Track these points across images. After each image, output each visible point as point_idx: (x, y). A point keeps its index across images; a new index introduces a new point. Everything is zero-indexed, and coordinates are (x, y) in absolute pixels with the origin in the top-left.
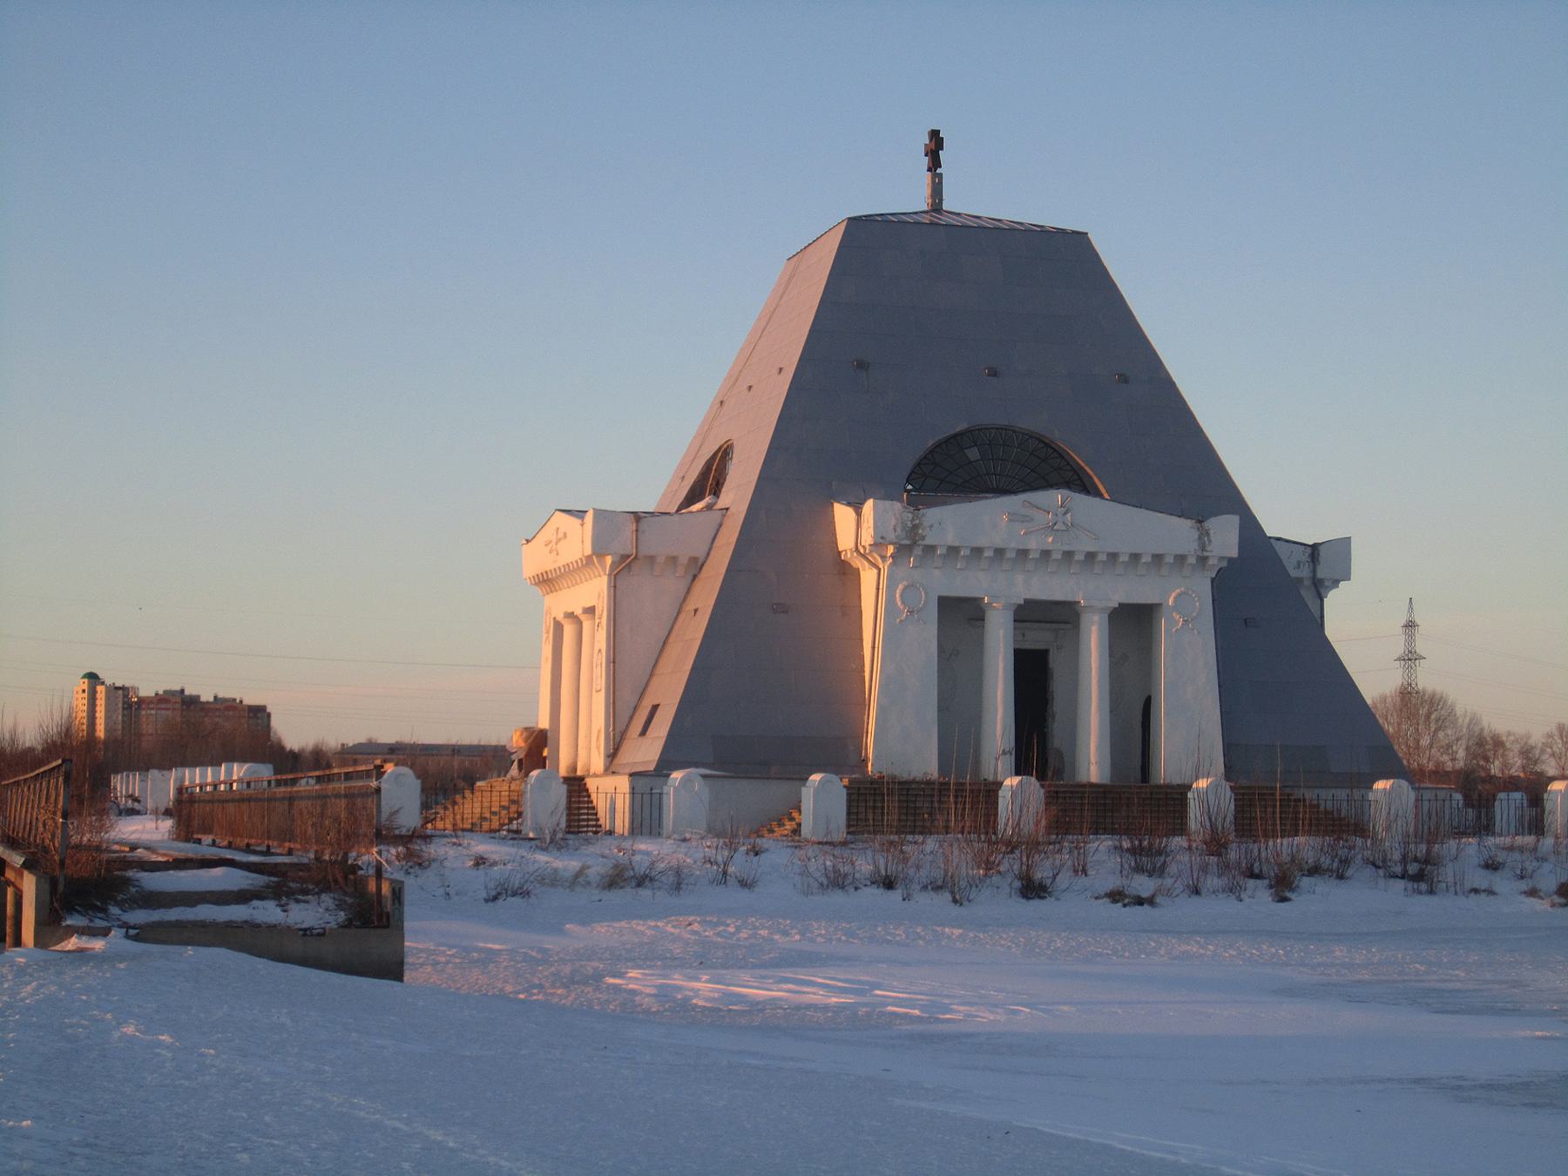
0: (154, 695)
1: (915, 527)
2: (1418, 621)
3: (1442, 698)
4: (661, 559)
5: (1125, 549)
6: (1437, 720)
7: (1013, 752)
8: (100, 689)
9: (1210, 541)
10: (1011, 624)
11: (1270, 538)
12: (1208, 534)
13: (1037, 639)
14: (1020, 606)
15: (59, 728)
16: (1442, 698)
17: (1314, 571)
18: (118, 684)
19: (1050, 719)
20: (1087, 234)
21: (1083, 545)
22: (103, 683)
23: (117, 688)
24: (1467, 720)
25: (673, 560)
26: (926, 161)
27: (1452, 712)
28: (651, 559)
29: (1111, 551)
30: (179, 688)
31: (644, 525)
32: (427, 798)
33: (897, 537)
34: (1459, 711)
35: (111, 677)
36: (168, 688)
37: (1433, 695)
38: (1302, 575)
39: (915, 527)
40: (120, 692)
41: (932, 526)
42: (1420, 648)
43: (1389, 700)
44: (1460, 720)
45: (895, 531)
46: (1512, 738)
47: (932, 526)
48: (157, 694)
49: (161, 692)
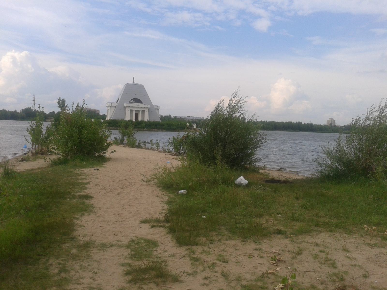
5: (141, 107)
20: (143, 85)
21: (139, 107)
25: (114, 106)
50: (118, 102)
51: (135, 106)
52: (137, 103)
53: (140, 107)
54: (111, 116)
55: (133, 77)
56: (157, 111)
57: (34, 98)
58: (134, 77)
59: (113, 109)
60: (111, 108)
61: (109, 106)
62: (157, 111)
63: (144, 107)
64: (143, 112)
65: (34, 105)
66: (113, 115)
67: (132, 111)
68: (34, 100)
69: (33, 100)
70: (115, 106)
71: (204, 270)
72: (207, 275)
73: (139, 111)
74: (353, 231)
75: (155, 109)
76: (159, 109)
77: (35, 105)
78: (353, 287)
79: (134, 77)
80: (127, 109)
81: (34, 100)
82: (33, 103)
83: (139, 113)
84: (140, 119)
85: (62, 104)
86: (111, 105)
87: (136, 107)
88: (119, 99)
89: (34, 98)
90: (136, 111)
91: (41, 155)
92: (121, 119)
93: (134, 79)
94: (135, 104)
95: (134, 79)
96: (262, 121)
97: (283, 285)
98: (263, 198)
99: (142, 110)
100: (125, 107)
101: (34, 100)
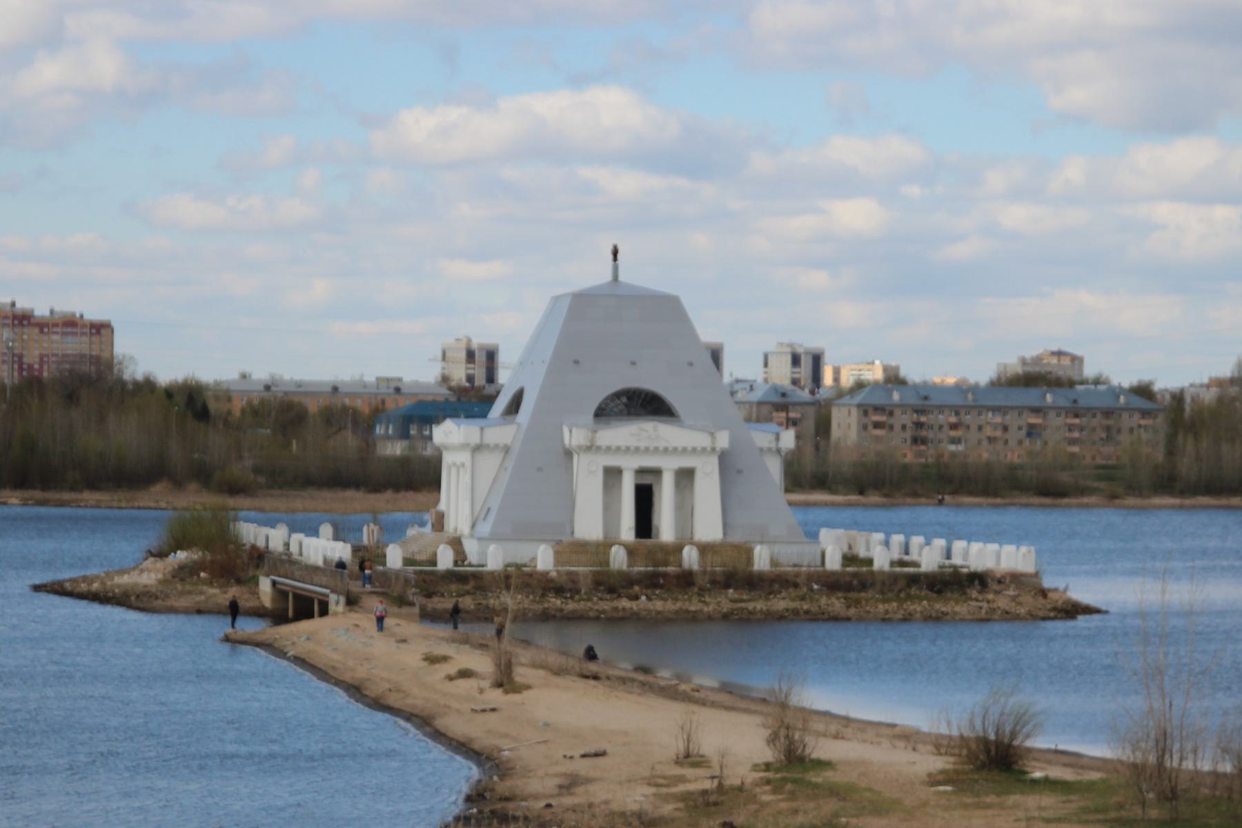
5: (671, 445)
13: (646, 480)
21: (661, 445)
25: (497, 446)
51: (633, 443)
54: (478, 508)
61: (468, 445)
63: (690, 445)
64: (685, 477)
67: (612, 475)
71: (25, 322)
73: (657, 472)
75: (761, 450)
81: (493, 710)
84: (666, 528)
85: (52, 312)
90: (641, 472)
91: (33, 365)
92: (216, 382)
96: (914, 373)
97: (209, 557)
98: (500, 588)
100: (568, 454)
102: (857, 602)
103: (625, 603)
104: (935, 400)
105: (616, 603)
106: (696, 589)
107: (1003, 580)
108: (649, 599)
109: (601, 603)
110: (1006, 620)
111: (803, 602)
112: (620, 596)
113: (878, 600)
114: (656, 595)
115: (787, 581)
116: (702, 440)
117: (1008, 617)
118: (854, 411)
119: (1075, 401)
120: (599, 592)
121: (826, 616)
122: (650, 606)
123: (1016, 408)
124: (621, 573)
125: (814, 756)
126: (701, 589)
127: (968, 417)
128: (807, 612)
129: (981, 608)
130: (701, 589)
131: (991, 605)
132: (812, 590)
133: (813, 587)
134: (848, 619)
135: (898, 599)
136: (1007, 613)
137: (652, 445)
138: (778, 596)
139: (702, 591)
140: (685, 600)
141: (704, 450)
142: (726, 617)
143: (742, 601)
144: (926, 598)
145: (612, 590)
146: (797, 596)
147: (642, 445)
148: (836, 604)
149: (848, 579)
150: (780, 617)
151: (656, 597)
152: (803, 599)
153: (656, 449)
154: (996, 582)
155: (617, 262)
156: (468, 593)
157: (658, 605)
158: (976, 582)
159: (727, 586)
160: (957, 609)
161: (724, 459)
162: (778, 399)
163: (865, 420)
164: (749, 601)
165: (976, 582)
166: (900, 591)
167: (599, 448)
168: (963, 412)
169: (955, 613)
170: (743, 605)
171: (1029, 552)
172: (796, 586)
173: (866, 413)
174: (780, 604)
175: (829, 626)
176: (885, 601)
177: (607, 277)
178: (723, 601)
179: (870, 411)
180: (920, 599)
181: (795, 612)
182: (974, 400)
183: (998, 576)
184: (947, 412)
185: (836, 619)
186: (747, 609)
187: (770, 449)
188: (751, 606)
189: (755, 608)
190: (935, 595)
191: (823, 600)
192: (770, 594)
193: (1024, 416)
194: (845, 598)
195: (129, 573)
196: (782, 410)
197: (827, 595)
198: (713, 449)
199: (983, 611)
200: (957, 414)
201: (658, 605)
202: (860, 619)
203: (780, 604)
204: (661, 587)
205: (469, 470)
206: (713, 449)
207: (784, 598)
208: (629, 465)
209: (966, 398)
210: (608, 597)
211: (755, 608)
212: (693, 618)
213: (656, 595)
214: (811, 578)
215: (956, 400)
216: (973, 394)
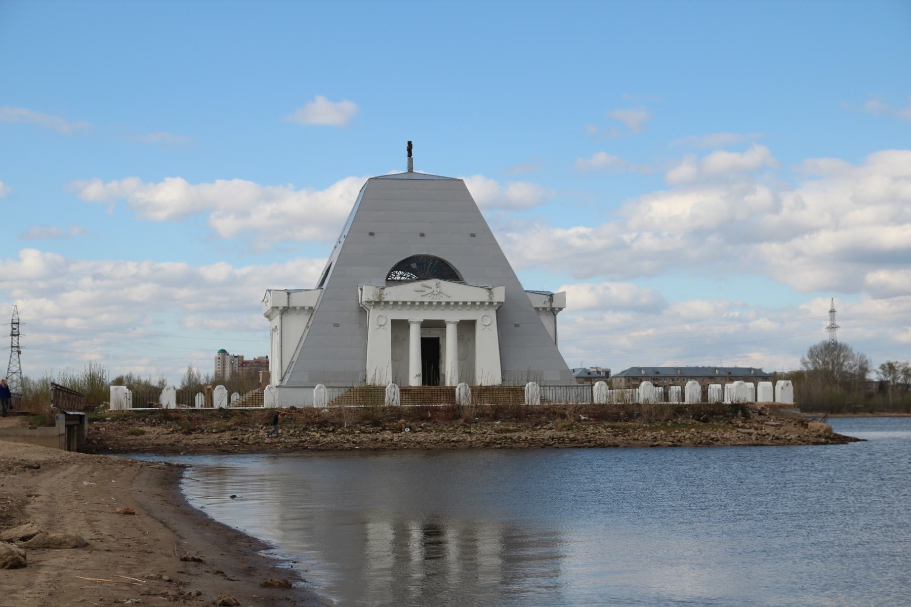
0: (253, 359)
1: (381, 295)
2: (836, 310)
3: (845, 346)
4: (298, 308)
5: (453, 300)
6: (844, 356)
7: (421, 375)
8: (227, 357)
9: (493, 296)
10: (420, 328)
11: (526, 291)
12: (493, 294)
13: (433, 334)
14: (422, 322)
15: (91, 377)
16: (845, 346)
17: (551, 305)
18: (236, 355)
19: (440, 363)
20: (462, 180)
21: (444, 300)
22: (228, 354)
23: (235, 357)
24: (859, 357)
25: (303, 308)
26: (407, 153)
27: (851, 350)
28: (295, 308)
29: (455, 301)
30: (265, 356)
31: (292, 295)
32: (443, 411)
33: (374, 298)
34: (855, 352)
35: (233, 351)
36: (260, 356)
37: (814, 346)
38: (546, 306)
39: (381, 295)
40: (237, 359)
41: (387, 294)
42: (838, 323)
43: (819, 348)
44: (856, 356)
45: (373, 296)
46: (897, 365)
47: (387, 294)
48: (255, 359)
49: (256, 358)
50: (325, 286)
51: (418, 298)
52: (432, 283)
53: (448, 303)
54: (285, 369)
55: (407, 145)
56: (546, 320)
57: (15, 326)
58: (410, 143)
59: (297, 326)
60: (285, 318)
61: (277, 308)
62: (546, 320)
64: (467, 328)
65: (15, 356)
66: (295, 359)
67: (400, 327)
68: (15, 334)
69: (13, 335)
70: (311, 308)
72: (723, 503)
74: (89, 432)
75: (537, 309)
76: (561, 309)
77: (19, 353)
78: (536, 544)
79: (410, 143)
80: (374, 315)
82: (12, 347)
83: (444, 336)
86: (283, 303)
87: (422, 303)
88: (331, 264)
89: (15, 326)
93: (410, 154)
94: (418, 285)
95: (410, 154)
99: (461, 321)
100: (362, 311)
101: (15, 332)
102: (625, 430)
103: (387, 435)
104: (662, 374)
105: (380, 436)
106: (462, 421)
107: (763, 412)
108: (412, 430)
109: (362, 435)
110: (778, 445)
111: (569, 432)
112: (384, 429)
113: (645, 429)
114: (421, 427)
115: (555, 413)
116: (481, 295)
117: (778, 442)
118: (623, 380)
119: (730, 373)
120: (363, 426)
121: (592, 444)
122: (411, 436)
123: (701, 377)
124: (393, 408)
125: (700, 398)
126: (467, 420)
127: (678, 381)
128: (573, 440)
129: (750, 434)
130: (467, 420)
131: (759, 432)
132: (579, 420)
133: (580, 418)
134: (616, 446)
135: (665, 427)
136: (777, 438)
137: (436, 299)
138: (545, 427)
139: (468, 422)
140: (450, 431)
141: (482, 303)
142: (488, 446)
143: (509, 431)
144: (693, 426)
145: (376, 423)
146: (565, 426)
147: (426, 299)
148: (603, 432)
149: (615, 410)
150: (545, 446)
151: (420, 429)
152: (570, 428)
153: (439, 303)
154: (757, 414)
155: (412, 157)
156: (229, 428)
157: (421, 436)
158: (740, 413)
159: (496, 418)
160: (727, 435)
161: (501, 310)
162: (587, 375)
163: (628, 384)
164: (515, 431)
165: (740, 413)
166: (667, 420)
167: (387, 303)
168: (676, 379)
169: (727, 439)
170: (508, 435)
171: (787, 385)
172: (563, 416)
173: (629, 380)
174: (545, 434)
175: (598, 453)
176: (651, 429)
177: (402, 169)
178: (489, 431)
179: (631, 379)
180: (687, 427)
181: (561, 440)
182: (681, 374)
183: (759, 408)
184: (668, 379)
185: (603, 446)
186: (511, 439)
187: (544, 309)
188: (516, 435)
189: (520, 437)
190: (702, 424)
191: (591, 429)
192: (536, 425)
193: (705, 381)
194: (613, 428)
195: (4, 428)
196: (588, 381)
197: (593, 425)
198: (491, 303)
199: (754, 437)
200: (673, 380)
201: (421, 436)
202: (628, 446)
203: (545, 434)
204: (428, 419)
205: (279, 332)
206: (491, 303)
207: (551, 429)
208: (415, 317)
209: (677, 373)
210: (371, 429)
211: (520, 437)
212: (454, 447)
213: (421, 427)
214: (578, 409)
215: (673, 373)
216: (680, 371)
